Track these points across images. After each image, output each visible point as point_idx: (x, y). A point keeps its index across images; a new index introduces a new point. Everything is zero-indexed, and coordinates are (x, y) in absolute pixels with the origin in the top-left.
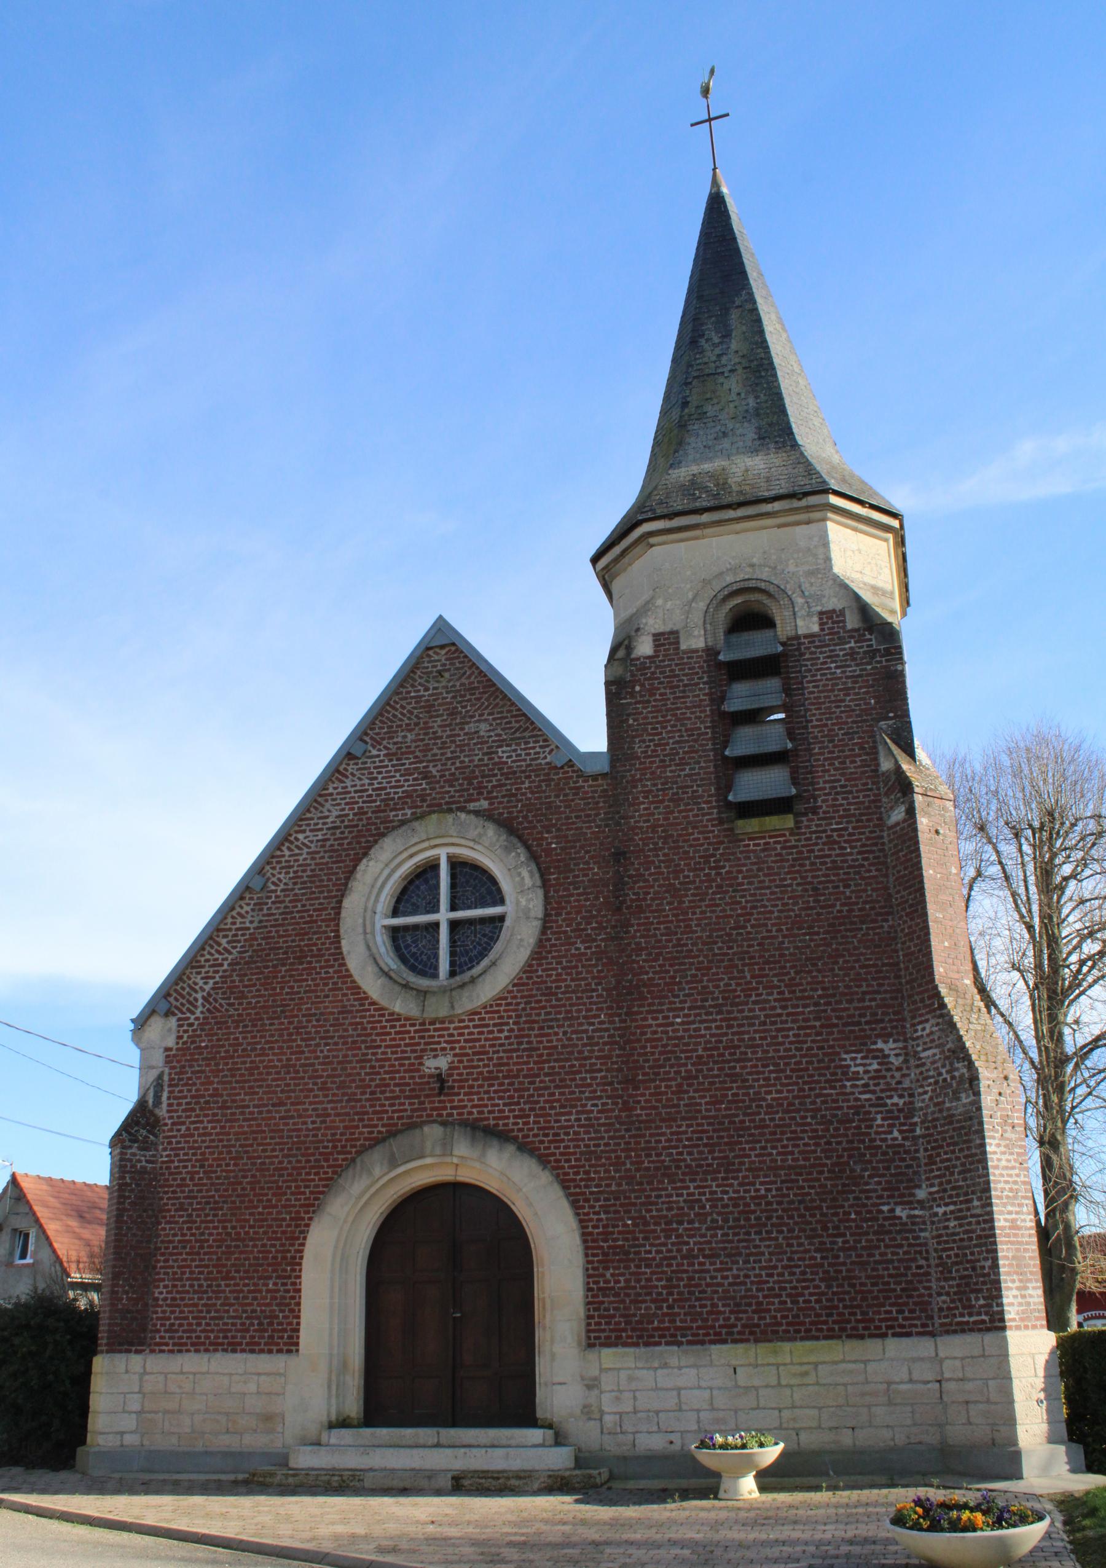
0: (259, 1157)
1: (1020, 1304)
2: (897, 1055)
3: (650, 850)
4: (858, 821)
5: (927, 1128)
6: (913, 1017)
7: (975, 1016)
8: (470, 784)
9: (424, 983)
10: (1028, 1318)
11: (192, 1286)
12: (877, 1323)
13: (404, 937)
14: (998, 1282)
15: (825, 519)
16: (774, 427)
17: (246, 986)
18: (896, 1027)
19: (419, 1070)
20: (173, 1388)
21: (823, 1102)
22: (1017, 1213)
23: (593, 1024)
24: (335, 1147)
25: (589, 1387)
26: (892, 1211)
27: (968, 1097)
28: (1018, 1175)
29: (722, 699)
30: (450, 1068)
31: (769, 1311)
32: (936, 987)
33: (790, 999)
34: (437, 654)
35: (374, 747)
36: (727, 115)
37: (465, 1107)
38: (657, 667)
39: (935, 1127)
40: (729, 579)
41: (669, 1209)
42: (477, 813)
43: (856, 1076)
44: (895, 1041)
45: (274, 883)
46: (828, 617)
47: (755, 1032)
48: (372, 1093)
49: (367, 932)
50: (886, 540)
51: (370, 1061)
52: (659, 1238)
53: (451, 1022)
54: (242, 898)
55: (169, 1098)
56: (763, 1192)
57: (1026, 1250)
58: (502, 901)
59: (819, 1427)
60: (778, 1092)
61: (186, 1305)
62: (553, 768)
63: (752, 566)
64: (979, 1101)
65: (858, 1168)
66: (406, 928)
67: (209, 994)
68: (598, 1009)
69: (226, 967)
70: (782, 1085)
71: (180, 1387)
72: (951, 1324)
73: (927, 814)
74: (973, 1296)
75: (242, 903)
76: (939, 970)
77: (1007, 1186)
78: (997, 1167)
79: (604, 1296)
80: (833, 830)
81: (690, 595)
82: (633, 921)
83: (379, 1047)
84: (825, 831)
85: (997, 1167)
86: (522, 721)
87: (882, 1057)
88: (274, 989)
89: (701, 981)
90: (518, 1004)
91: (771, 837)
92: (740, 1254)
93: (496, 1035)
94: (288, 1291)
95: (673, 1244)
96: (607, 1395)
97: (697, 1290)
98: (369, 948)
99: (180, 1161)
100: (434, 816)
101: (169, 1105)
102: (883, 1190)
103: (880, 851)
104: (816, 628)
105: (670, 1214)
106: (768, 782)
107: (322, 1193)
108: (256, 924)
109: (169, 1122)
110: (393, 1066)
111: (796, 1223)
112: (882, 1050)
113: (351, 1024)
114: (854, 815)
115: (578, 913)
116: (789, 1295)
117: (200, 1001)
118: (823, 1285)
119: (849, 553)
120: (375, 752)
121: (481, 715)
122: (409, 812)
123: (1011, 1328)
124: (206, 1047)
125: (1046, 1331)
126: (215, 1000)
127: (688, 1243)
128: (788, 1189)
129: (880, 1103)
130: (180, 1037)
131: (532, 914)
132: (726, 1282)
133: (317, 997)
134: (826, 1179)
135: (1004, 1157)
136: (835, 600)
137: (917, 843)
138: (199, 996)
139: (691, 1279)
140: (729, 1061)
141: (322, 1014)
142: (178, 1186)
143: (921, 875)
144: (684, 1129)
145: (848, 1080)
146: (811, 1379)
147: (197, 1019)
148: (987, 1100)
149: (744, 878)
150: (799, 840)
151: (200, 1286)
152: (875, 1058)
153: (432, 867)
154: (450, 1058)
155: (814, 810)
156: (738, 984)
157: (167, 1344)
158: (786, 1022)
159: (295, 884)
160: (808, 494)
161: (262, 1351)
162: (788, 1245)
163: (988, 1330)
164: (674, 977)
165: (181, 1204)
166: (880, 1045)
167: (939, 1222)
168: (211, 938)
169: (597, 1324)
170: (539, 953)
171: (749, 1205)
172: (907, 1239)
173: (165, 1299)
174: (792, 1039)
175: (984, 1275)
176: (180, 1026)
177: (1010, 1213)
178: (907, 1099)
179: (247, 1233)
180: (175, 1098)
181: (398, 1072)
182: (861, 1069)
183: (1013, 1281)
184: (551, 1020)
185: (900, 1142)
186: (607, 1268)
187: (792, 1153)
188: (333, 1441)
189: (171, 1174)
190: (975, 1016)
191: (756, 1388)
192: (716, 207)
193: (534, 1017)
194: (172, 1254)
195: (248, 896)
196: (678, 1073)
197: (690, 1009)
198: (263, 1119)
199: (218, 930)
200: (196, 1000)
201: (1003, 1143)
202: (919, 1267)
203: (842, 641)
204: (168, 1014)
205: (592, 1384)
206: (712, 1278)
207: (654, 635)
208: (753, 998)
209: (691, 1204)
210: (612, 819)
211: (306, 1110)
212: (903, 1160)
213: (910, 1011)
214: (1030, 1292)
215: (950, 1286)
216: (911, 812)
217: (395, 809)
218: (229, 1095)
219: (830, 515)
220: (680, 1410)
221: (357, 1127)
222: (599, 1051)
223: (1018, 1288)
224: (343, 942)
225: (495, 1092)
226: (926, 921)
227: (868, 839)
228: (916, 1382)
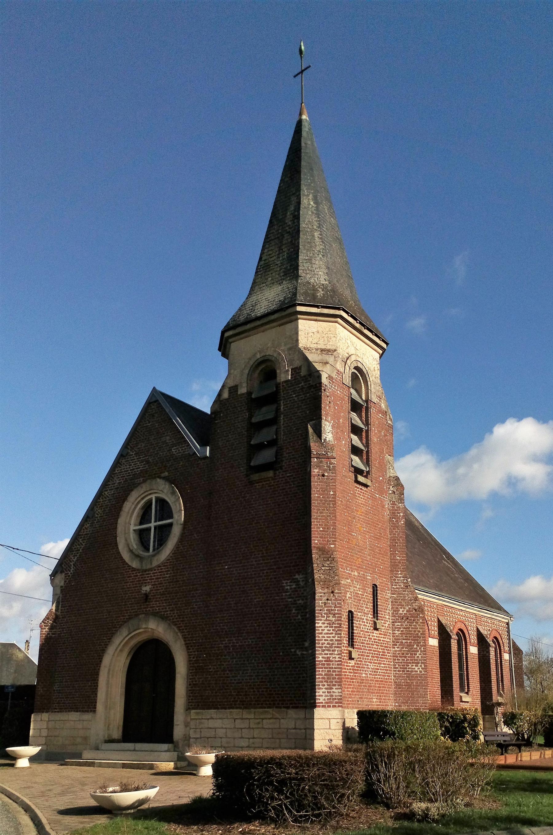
1: (326, 696)
15: (297, 319)
19: (140, 592)
21: (274, 603)
26: (295, 652)
34: (153, 405)
35: (131, 450)
36: (295, 77)
42: (164, 478)
44: (302, 574)
49: (126, 533)
53: (152, 571)
58: (171, 516)
60: (259, 598)
69: (81, 551)
75: (86, 523)
77: (326, 642)
81: (243, 366)
87: (297, 582)
91: (264, 482)
98: (126, 540)
100: (149, 481)
101: (61, 610)
106: (267, 456)
112: (297, 579)
116: (257, 688)
118: (268, 684)
119: (310, 335)
121: (167, 433)
130: (65, 582)
132: (323, 673)
134: (273, 637)
136: (298, 362)
138: (72, 564)
147: (71, 573)
152: (294, 582)
153: (150, 501)
161: (86, 711)
162: (258, 666)
166: (297, 576)
169: (192, 699)
172: (300, 664)
176: (66, 577)
178: (305, 601)
182: (288, 587)
191: (241, 729)
201: (326, 622)
202: (303, 677)
204: (61, 572)
205: (187, 725)
207: (230, 388)
217: (137, 478)
224: (118, 538)
228: (298, 729)
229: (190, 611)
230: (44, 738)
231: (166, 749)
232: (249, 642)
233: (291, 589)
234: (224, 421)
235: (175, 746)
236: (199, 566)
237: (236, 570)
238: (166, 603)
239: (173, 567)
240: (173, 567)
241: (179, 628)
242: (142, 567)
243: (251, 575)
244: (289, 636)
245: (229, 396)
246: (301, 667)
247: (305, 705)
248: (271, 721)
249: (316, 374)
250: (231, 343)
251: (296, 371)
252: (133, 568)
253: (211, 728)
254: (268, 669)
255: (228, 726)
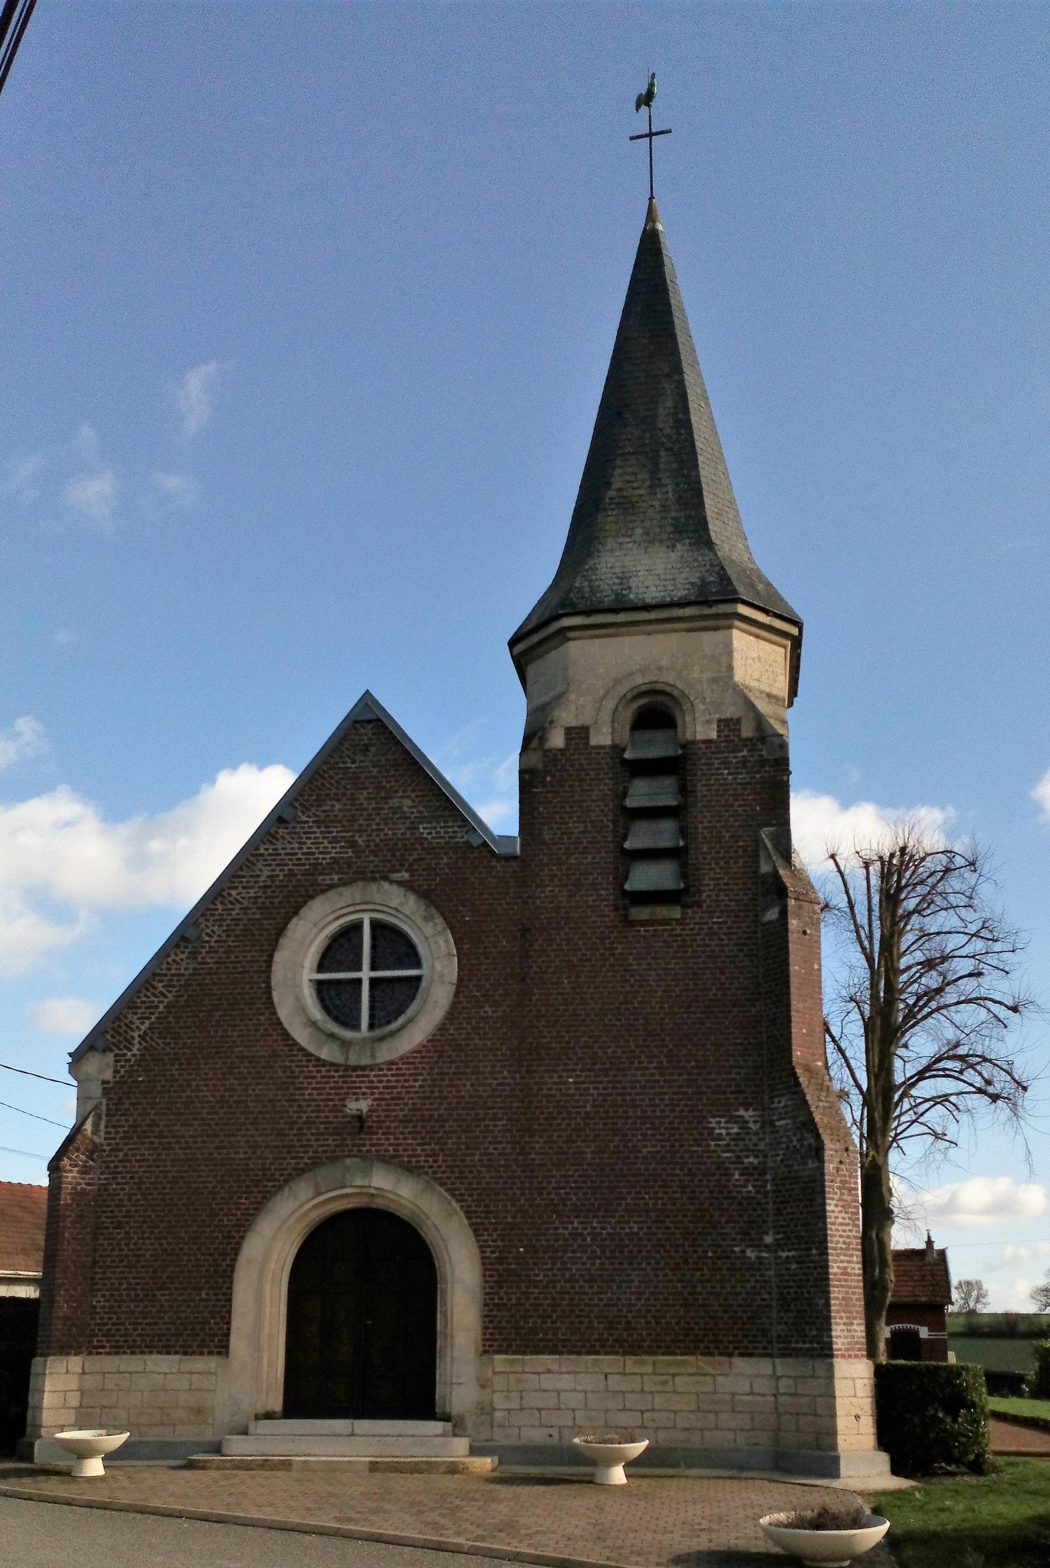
0: (195, 1182)
2: (755, 1122)
3: (553, 929)
4: (736, 916)
5: (776, 1185)
6: (772, 1091)
7: (824, 1094)
8: (393, 855)
9: (348, 1034)
10: (852, 1349)
11: (128, 1295)
12: (726, 1344)
13: (328, 990)
14: (829, 1318)
15: (731, 627)
16: (689, 522)
17: (181, 1028)
18: (756, 1098)
20: (110, 1385)
22: (848, 1262)
23: (496, 1079)
24: (264, 1175)
25: (483, 1387)
26: (743, 1252)
27: (813, 1163)
28: (850, 1231)
29: (625, 794)
30: (369, 1111)
31: (636, 1329)
32: (793, 1068)
33: (667, 1068)
34: (364, 728)
35: (303, 813)
36: (632, 138)
37: (383, 1144)
38: (567, 760)
39: (783, 1185)
40: (639, 680)
41: (557, 1240)
42: (400, 883)
43: (719, 1137)
44: (755, 1110)
45: (208, 935)
46: (728, 725)
47: (636, 1094)
48: (299, 1129)
50: (785, 647)
51: (298, 1100)
52: (547, 1264)
53: (372, 1070)
54: (177, 946)
55: (106, 1127)
56: (635, 1230)
57: (854, 1293)
58: (418, 964)
59: (675, 1427)
61: (123, 1312)
62: (468, 845)
63: (659, 668)
64: (823, 1168)
65: (716, 1214)
66: (330, 982)
67: (145, 1032)
68: (501, 1066)
69: (161, 1009)
70: (656, 1140)
71: (117, 1385)
72: (787, 1349)
73: (799, 916)
74: (807, 1327)
75: (178, 951)
76: (797, 1053)
77: (841, 1240)
78: (833, 1224)
79: (498, 1310)
80: (714, 923)
81: (602, 692)
82: (535, 991)
83: (306, 1089)
84: (706, 923)
85: (833, 1224)
86: (445, 804)
87: (743, 1123)
88: (209, 1032)
89: (592, 1047)
90: (431, 1058)
92: (613, 1281)
93: (412, 1083)
94: (219, 1300)
95: (558, 1269)
96: (498, 1394)
97: (577, 1309)
99: (118, 1184)
100: (360, 884)
101: (107, 1133)
102: (737, 1234)
103: (754, 944)
104: (714, 735)
105: (557, 1244)
107: (252, 1215)
108: (191, 971)
109: (108, 1148)
110: (318, 1106)
111: (662, 1258)
112: (742, 1117)
113: (280, 1067)
114: (733, 911)
115: (486, 980)
117: (137, 1039)
120: (304, 818)
122: (336, 877)
123: (837, 1356)
124: (142, 1081)
125: (865, 1360)
126: (152, 1039)
127: (570, 1269)
128: (657, 1228)
129: (738, 1160)
130: (116, 1072)
131: (447, 979)
133: (248, 1041)
134: (690, 1222)
135: (840, 1215)
136: (733, 709)
137: (787, 942)
139: (572, 1299)
140: (612, 1118)
141: (253, 1057)
142: (117, 1206)
143: (788, 970)
144: (570, 1173)
145: (713, 1140)
146: (669, 1388)
147: (134, 1055)
148: (830, 1167)
149: (634, 959)
150: (684, 930)
151: (137, 1295)
152: (736, 1122)
154: (370, 1102)
155: (699, 904)
156: (624, 1052)
157: (104, 1347)
158: (663, 1087)
159: (228, 936)
160: (718, 598)
161: (193, 1353)
163: (819, 1356)
164: (568, 1042)
165: (119, 1222)
166: (742, 1112)
167: (782, 1263)
168: (147, 982)
169: (491, 1334)
170: (452, 1015)
171: (623, 1240)
173: (103, 1307)
174: (667, 1102)
175: (818, 1311)
177: (842, 1262)
178: (761, 1159)
179: (181, 1249)
180: (113, 1127)
181: (323, 1111)
182: (723, 1132)
183: (841, 1318)
184: (461, 1073)
185: (753, 1195)
186: (501, 1288)
187: (662, 1198)
188: (259, 1431)
189: (109, 1195)
190: (824, 1094)
191: (623, 1393)
192: (650, 249)
193: (445, 1070)
194: (109, 1267)
195: (182, 944)
196: (569, 1125)
197: (582, 1070)
198: (198, 1148)
199: (155, 975)
200: (133, 1038)
201: (840, 1203)
202: (763, 1300)
203: (736, 750)
204: (106, 1050)
205: (483, 1385)
206: (590, 1299)
208: (636, 1065)
209: (574, 1235)
210: (521, 897)
211: (239, 1142)
212: (755, 1210)
213: (770, 1086)
214: (855, 1327)
215: (789, 1318)
216: (784, 913)
217: (321, 874)
218: (165, 1126)
219: (737, 623)
220: (559, 1409)
221: (285, 1158)
222: (502, 1102)
223: (845, 1324)
225: (409, 1133)
226: (789, 1011)
227: (744, 932)
229: (480, 1160)
230: (73, 1411)
231: (440, 1431)
232: (631, 1228)
233: (727, 1134)
234: (557, 792)
235: (455, 1426)
236: (501, 1072)
237: (596, 1088)
238: (414, 1139)
239: (432, 1068)
240: (432, 1068)
241: (451, 1191)
242: (347, 1059)
243: (634, 1100)
244: (727, 1222)
245: (567, 745)
246: (757, 1281)
247: (769, 1351)
248: (694, 1379)
249: (777, 741)
250: (572, 639)
251: (728, 725)
252: (318, 1059)
253: (546, 1391)
254: (679, 1281)
255: (589, 1388)
